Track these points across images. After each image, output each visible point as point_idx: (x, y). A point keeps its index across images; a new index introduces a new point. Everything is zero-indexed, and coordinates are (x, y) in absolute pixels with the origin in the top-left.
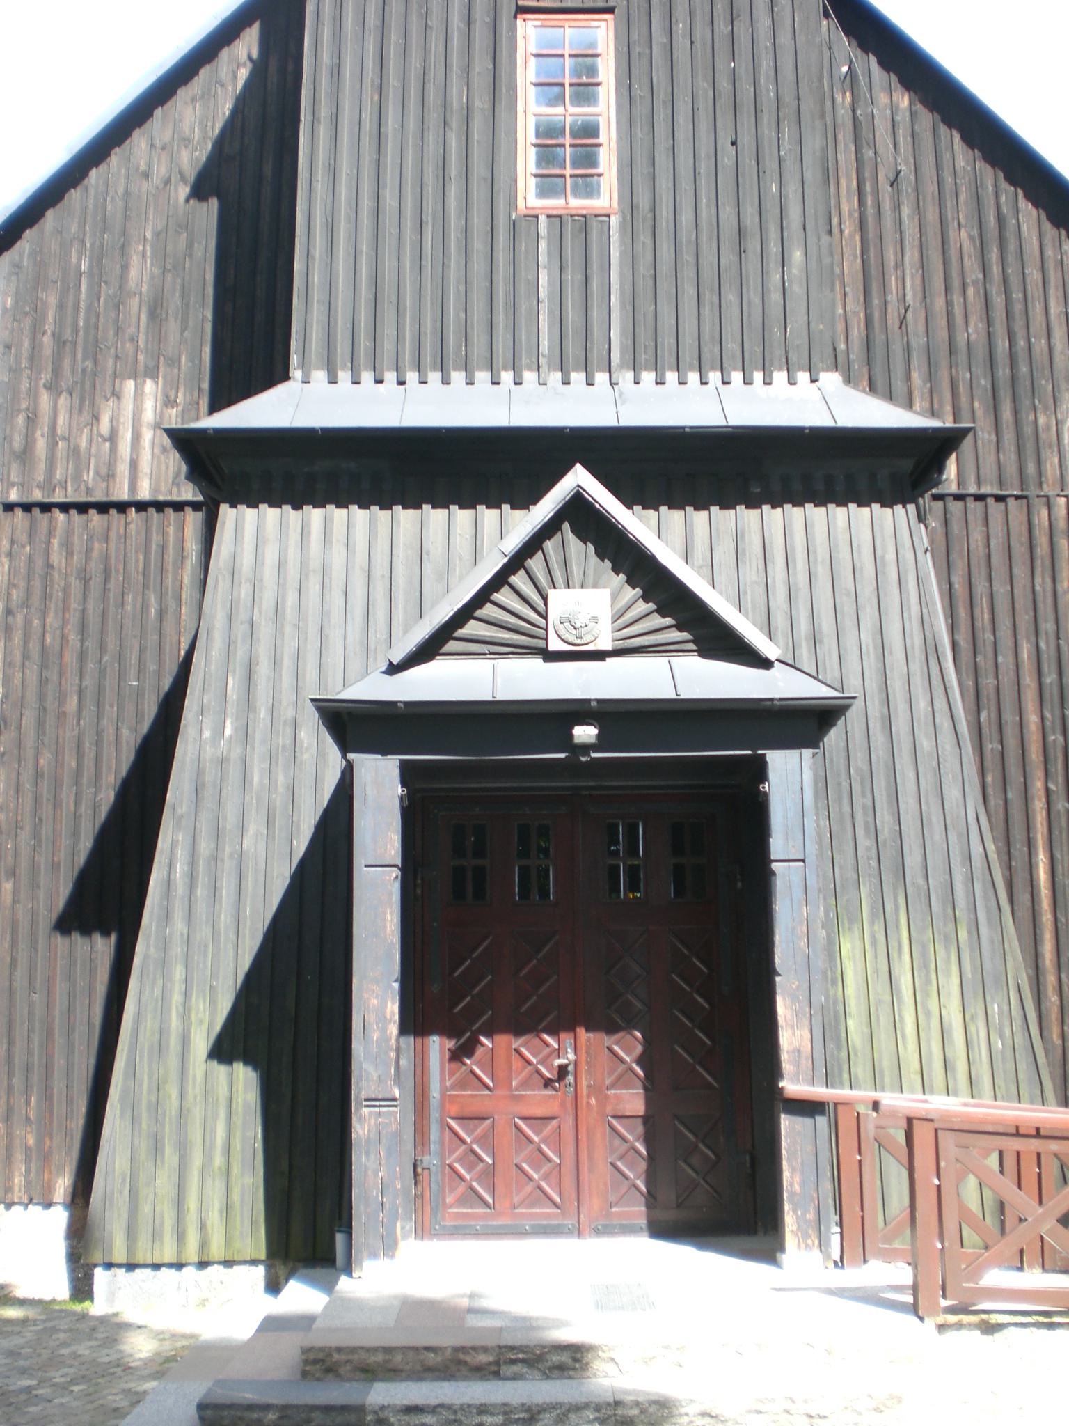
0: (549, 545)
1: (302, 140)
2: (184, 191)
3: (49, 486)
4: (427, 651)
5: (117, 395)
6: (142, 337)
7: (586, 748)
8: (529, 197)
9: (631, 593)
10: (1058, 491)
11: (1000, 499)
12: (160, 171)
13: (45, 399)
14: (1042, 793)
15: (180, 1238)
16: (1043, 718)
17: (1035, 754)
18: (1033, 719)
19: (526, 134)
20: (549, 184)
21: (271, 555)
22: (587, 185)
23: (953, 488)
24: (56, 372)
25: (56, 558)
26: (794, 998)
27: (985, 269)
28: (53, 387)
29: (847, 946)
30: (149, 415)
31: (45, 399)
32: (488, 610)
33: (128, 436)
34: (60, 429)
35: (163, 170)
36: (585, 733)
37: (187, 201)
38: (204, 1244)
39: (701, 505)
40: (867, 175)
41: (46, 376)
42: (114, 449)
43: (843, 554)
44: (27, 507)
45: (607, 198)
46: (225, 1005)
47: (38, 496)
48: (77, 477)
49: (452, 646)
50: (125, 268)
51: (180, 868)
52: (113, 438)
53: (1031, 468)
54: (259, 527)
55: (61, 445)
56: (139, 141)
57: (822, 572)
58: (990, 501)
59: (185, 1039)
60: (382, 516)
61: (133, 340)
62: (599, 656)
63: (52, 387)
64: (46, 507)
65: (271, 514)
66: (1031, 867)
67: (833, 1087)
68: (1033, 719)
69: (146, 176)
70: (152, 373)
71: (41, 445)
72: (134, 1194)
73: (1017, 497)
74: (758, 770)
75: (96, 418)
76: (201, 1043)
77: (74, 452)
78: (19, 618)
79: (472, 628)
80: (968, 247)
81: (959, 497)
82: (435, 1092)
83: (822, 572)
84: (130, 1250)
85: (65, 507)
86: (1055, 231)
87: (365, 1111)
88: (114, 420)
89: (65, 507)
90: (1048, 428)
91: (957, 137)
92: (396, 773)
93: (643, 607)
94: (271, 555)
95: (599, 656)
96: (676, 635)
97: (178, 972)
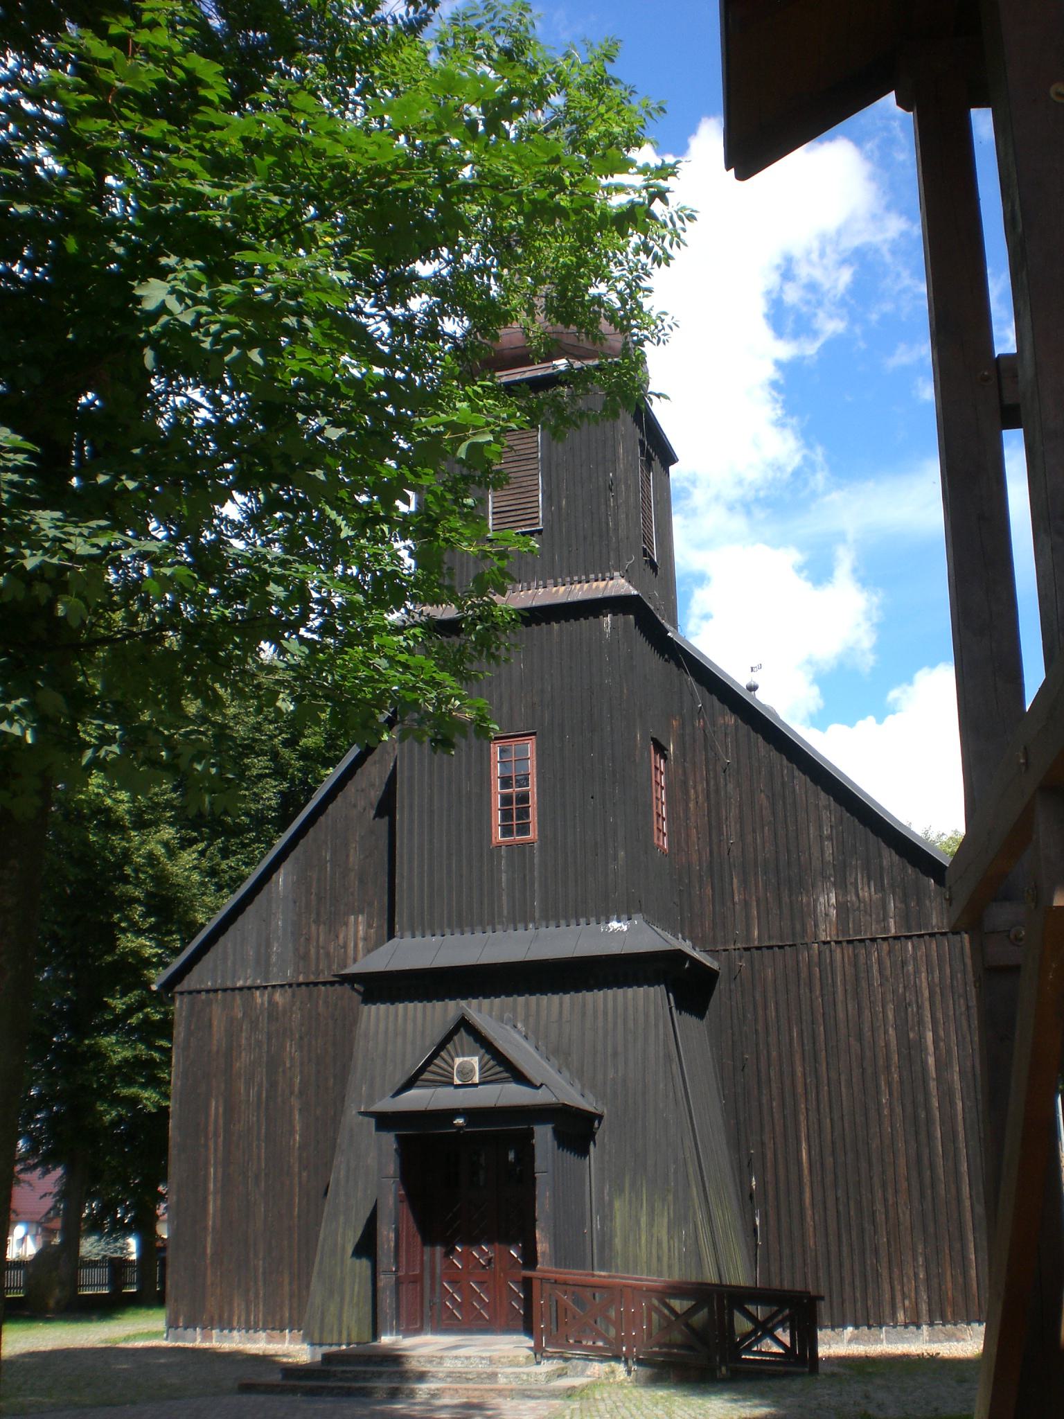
0: (456, 1038)
1: (398, 817)
2: (373, 813)
3: (318, 973)
4: (409, 1084)
5: (346, 924)
6: (356, 893)
7: (460, 1127)
8: (498, 836)
9: (487, 1057)
10: (813, 940)
11: (780, 947)
12: (362, 804)
13: (313, 927)
14: (804, 1111)
15: (340, 1333)
16: (804, 1069)
17: (800, 1089)
18: (799, 1070)
19: (497, 802)
20: (507, 831)
21: (382, 1026)
22: (524, 829)
23: (756, 944)
24: (318, 914)
25: (321, 1009)
26: (542, 1230)
27: (774, 813)
28: (317, 922)
29: (617, 1204)
30: (361, 934)
31: (313, 927)
32: (432, 1068)
33: (352, 945)
34: (321, 943)
35: (363, 803)
36: (459, 1121)
37: (374, 818)
38: (349, 1335)
39: (566, 992)
40: (711, 767)
41: (313, 916)
42: (346, 952)
43: (631, 1011)
44: (307, 984)
45: (533, 835)
46: (359, 1233)
47: (312, 978)
48: (329, 968)
49: (418, 1083)
50: (347, 856)
51: (342, 1173)
52: (345, 946)
53: (798, 927)
54: (378, 1014)
55: (322, 951)
56: (351, 787)
57: (620, 1021)
58: (776, 949)
59: (344, 1248)
60: (429, 1005)
61: (352, 894)
62: (475, 1085)
63: (317, 922)
64: (316, 984)
65: (382, 1007)
66: (799, 1151)
67: (569, 1268)
68: (799, 1070)
69: (355, 806)
70: (361, 911)
71: (313, 951)
72: (323, 1313)
73: (790, 946)
74: (531, 1134)
75: (337, 937)
76: (350, 1249)
77: (328, 954)
78: (306, 1040)
79: (426, 1076)
80: (765, 803)
81: (758, 948)
82: (438, 1271)
83: (620, 1021)
84: (321, 1338)
85: (324, 983)
86: (814, 787)
87: (382, 1277)
88: (346, 937)
89: (324, 983)
90: (809, 904)
91: (761, 739)
92: (393, 1139)
93: (492, 1063)
94: (382, 1026)
95: (475, 1085)
96: (506, 1075)
97: (342, 1219)
